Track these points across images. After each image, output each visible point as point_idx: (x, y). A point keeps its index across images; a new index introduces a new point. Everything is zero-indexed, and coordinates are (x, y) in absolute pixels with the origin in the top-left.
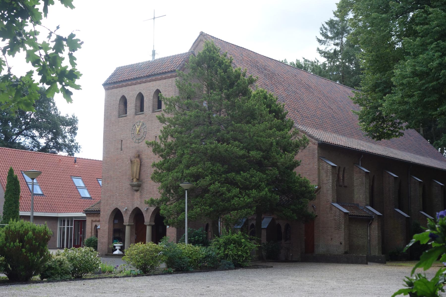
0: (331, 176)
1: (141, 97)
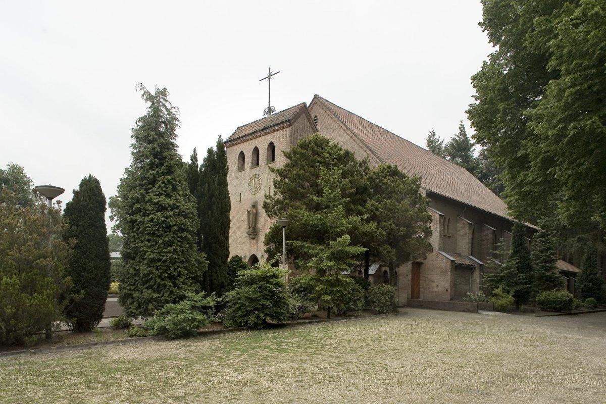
0: (438, 225)
1: (256, 151)
